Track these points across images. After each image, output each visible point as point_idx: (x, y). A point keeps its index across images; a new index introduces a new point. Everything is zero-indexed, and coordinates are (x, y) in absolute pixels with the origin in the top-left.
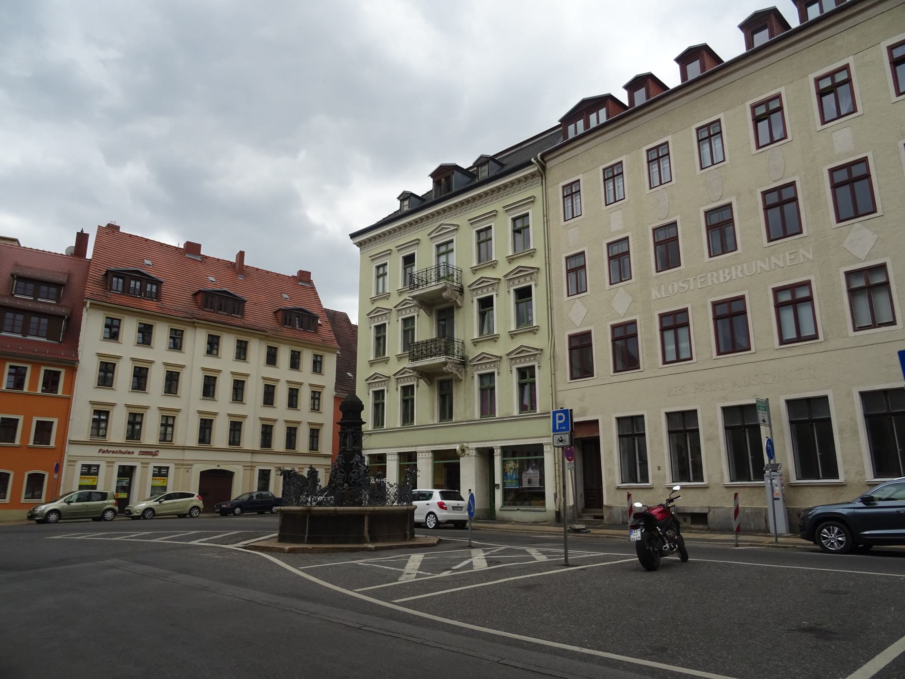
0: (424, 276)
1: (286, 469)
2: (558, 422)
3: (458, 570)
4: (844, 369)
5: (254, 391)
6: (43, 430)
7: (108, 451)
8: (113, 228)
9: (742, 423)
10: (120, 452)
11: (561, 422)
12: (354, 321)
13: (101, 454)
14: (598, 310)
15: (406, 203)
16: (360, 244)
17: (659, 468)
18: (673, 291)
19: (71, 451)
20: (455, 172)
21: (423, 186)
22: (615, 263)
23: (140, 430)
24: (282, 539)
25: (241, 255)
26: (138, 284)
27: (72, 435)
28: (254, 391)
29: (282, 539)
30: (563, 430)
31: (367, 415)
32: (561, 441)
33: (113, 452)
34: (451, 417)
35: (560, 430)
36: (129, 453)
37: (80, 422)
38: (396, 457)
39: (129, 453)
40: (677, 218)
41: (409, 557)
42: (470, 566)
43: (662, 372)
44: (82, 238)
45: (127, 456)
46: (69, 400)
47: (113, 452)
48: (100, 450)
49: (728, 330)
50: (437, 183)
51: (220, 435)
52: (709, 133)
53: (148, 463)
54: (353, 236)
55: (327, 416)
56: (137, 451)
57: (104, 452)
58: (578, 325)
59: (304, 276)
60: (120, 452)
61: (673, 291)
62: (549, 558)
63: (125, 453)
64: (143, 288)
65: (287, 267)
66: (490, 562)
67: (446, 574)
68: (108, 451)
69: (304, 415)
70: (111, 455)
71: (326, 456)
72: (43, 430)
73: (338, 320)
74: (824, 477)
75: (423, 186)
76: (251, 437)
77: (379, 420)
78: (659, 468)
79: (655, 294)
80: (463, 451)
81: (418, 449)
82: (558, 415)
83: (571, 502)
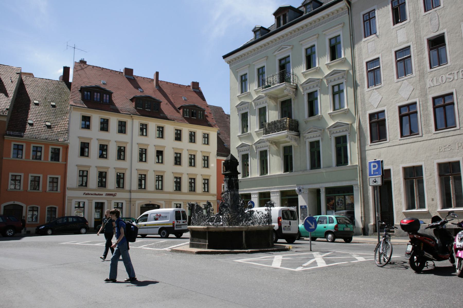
0: (271, 80)
1: (192, 203)
2: (372, 169)
3: (306, 267)
4: (429, 150)
5: (169, 157)
6: (54, 181)
7: (88, 194)
8: (83, 62)
9: (413, 175)
10: (95, 194)
11: (375, 169)
12: (227, 111)
13: (85, 196)
14: (387, 97)
15: (258, 33)
16: (229, 62)
17: (433, 200)
18: (442, 81)
19: (69, 193)
20: (290, 10)
21: (269, 21)
22: (371, 74)
23: (105, 182)
24: (192, 246)
25: (157, 74)
26: (99, 94)
27: (68, 185)
28: (169, 157)
29: (192, 246)
30: (376, 175)
31: (239, 168)
32: (375, 182)
33: (92, 194)
34: (346, 162)
35: (374, 175)
36: (100, 195)
37: (73, 179)
38: (278, 194)
39: (100, 195)
40: (445, 31)
41: (273, 258)
42: (315, 263)
43: (435, 136)
44: (66, 70)
45: (99, 196)
46: (66, 165)
47: (92, 194)
48: (84, 194)
49: (443, 113)
50: (278, 19)
51: (151, 183)
52: (369, 17)
53: (111, 201)
54: (224, 57)
55: (212, 172)
56: (104, 193)
57: (86, 194)
58: (376, 107)
59: (195, 85)
60: (95, 194)
61: (442, 81)
62: (366, 259)
63: (98, 195)
64: (102, 97)
65: (186, 81)
66: (327, 262)
67: (299, 269)
68: (88, 194)
69: (199, 171)
70: (90, 196)
71: (213, 195)
72: (54, 181)
73: (219, 110)
74: (165, 208)
75: (269, 21)
76: (169, 184)
77: (246, 173)
78: (433, 200)
79: (429, 83)
80: (300, 190)
81: (251, 192)
82: (372, 164)
83: (372, 222)
